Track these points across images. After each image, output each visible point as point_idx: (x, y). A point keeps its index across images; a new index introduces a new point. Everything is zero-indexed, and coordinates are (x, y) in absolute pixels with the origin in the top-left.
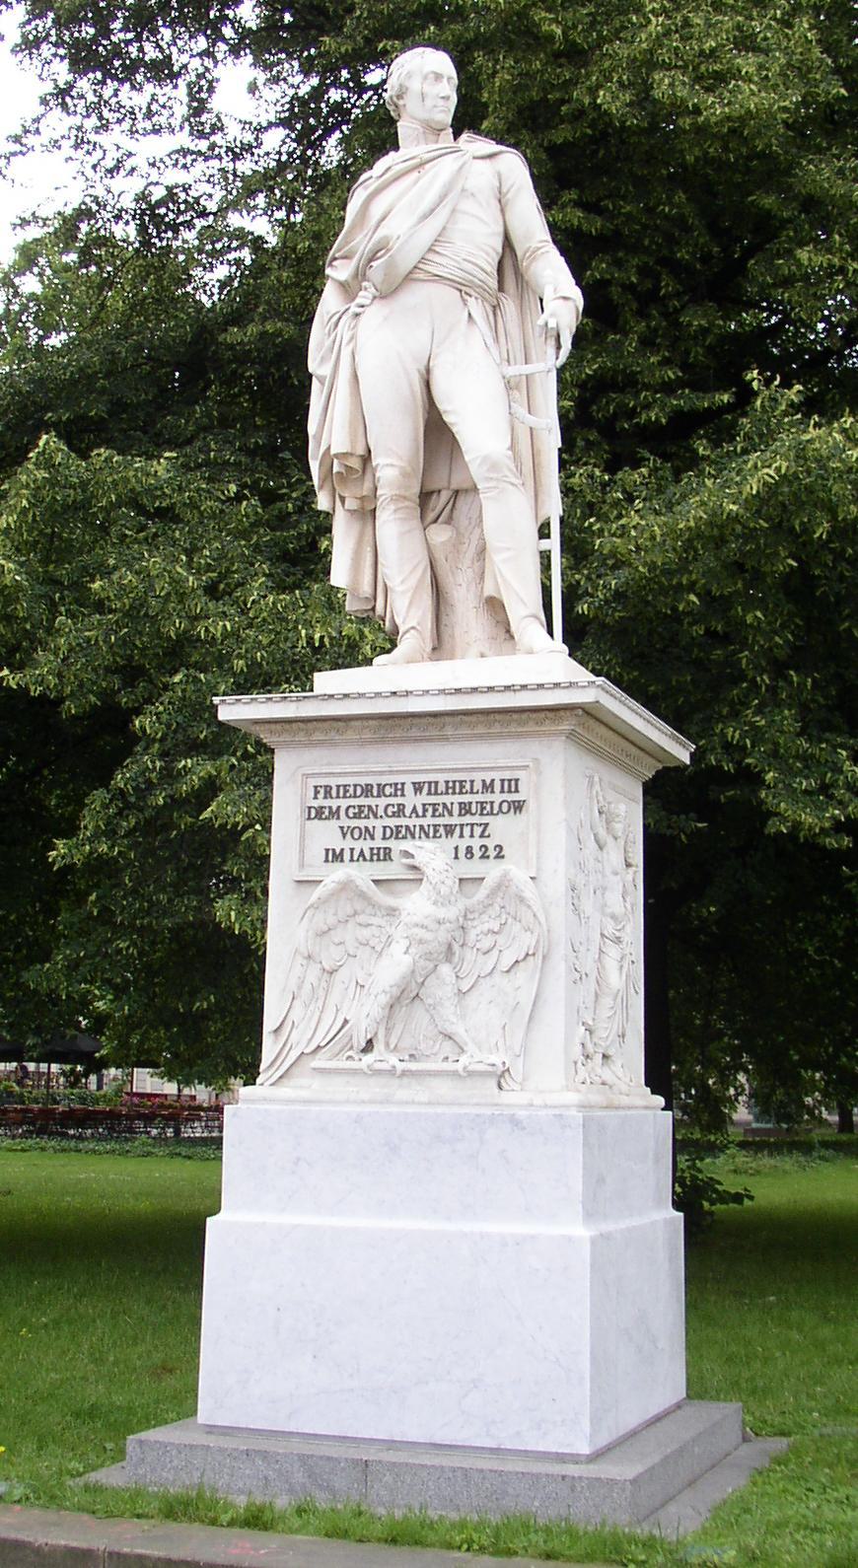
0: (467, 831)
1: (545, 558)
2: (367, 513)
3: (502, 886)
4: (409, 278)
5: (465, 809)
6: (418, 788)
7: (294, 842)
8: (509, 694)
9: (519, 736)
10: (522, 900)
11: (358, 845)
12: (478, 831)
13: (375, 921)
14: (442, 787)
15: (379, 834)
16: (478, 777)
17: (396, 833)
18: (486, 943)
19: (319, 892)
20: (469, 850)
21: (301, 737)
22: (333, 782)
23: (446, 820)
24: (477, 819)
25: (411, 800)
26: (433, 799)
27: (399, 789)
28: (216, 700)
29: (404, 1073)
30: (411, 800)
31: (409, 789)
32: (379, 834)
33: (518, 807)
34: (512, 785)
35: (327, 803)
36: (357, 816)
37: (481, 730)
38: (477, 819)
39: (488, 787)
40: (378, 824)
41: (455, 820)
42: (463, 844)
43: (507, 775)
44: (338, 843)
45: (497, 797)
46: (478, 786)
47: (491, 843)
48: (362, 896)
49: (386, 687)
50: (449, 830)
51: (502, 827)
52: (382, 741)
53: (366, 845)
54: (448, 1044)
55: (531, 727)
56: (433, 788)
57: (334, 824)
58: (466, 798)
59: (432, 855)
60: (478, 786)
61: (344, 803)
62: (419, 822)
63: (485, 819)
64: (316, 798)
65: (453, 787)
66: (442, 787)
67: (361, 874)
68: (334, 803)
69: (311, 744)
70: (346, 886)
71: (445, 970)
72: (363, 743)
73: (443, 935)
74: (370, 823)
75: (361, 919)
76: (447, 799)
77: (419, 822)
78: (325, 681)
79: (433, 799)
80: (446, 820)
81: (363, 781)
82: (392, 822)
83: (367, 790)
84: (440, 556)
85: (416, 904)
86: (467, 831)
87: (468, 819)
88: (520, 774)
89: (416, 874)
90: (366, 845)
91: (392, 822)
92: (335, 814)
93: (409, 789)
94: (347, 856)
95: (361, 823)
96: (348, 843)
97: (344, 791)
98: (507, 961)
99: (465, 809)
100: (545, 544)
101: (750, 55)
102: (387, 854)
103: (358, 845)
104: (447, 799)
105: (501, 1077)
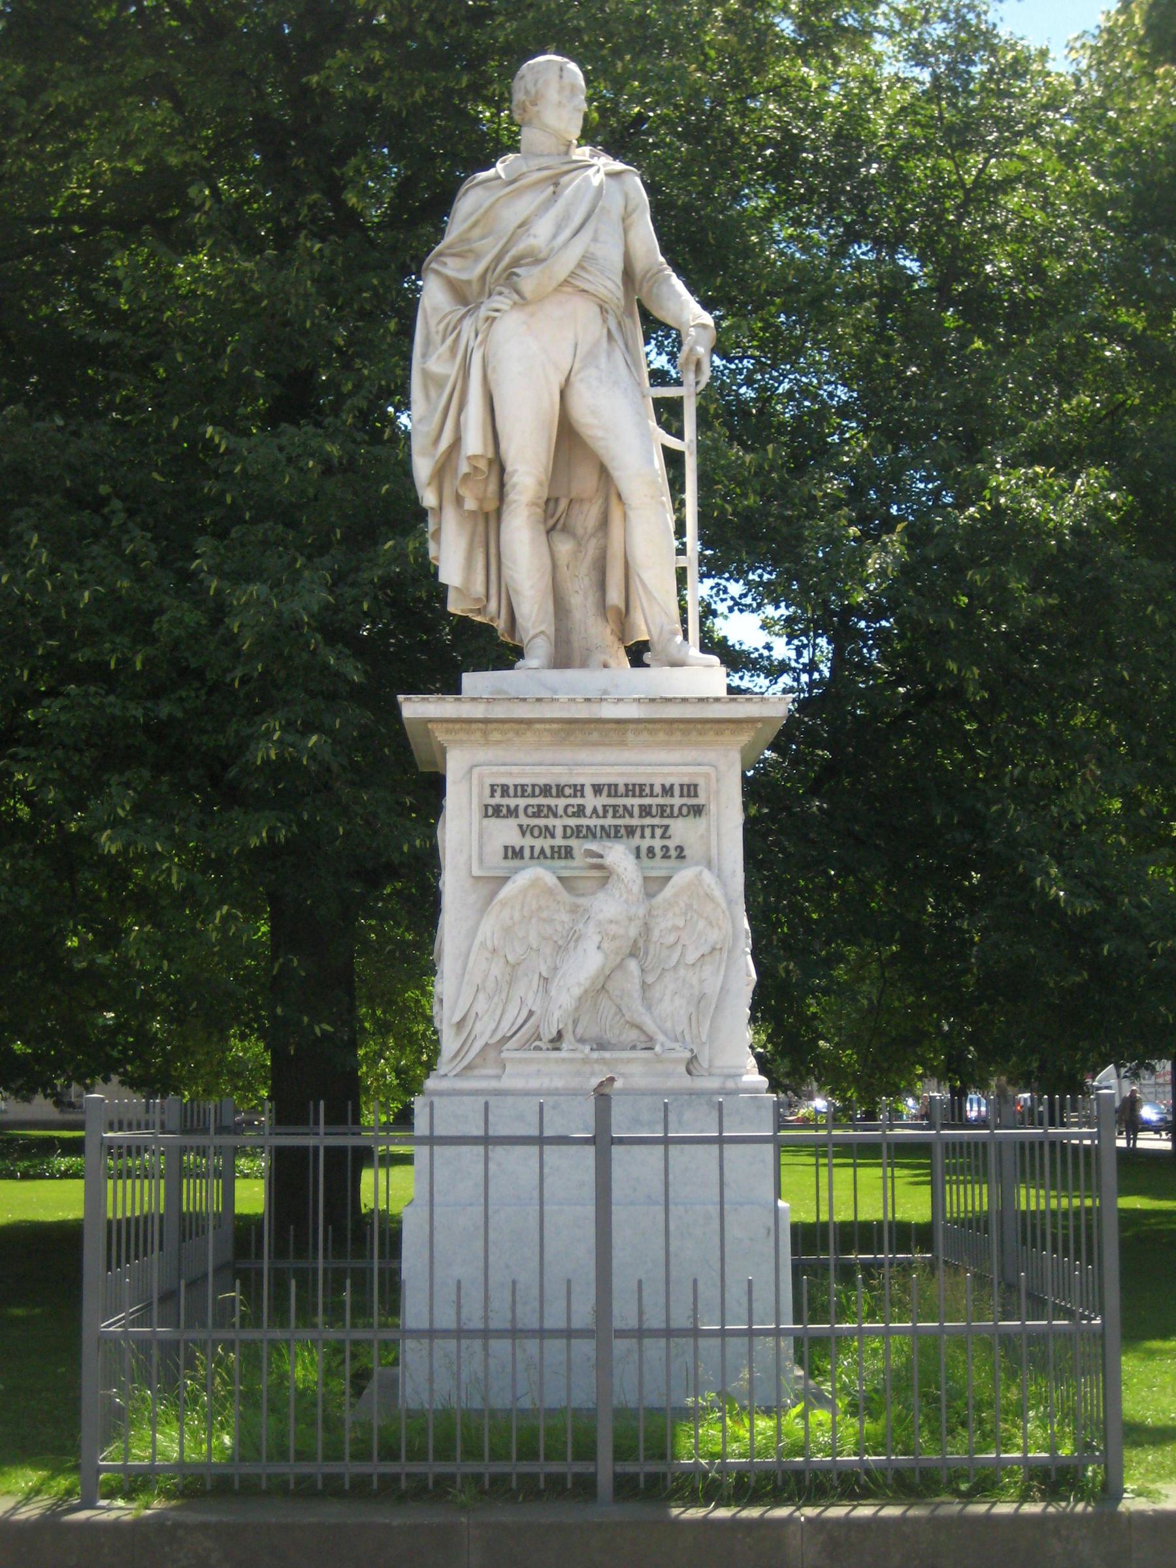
0: (648, 832)
2: (489, 520)
5: (645, 811)
6: (597, 789)
7: (463, 836)
11: (538, 843)
12: (659, 832)
14: (621, 789)
15: (559, 832)
17: (577, 832)
20: (651, 851)
22: (510, 781)
23: (627, 821)
24: (656, 821)
27: (578, 790)
28: (401, 697)
30: (591, 801)
31: (588, 791)
33: (698, 811)
35: (505, 801)
38: (656, 821)
39: (668, 791)
41: (635, 822)
42: (645, 844)
43: (686, 781)
44: (516, 840)
45: (677, 801)
50: (631, 831)
51: (682, 830)
56: (613, 790)
57: (512, 822)
58: (647, 801)
59: (618, 855)
61: (522, 802)
62: (601, 822)
63: (666, 822)
64: (492, 796)
66: (621, 789)
68: (512, 802)
71: (633, 965)
73: (633, 932)
74: (550, 822)
76: (629, 801)
77: (601, 822)
80: (627, 821)
82: (573, 822)
83: (546, 790)
85: (608, 907)
86: (648, 832)
87: (648, 821)
88: (701, 782)
89: (604, 875)
91: (573, 822)
92: (512, 812)
93: (588, 791)
94: (527, 853)
95: (541, 822)
96: (528, 841)
97: (522, 790)
99: (645, 811)
100: (683, 561)
102: (568, 853)
103: (538, 843)
104: (629, 801)
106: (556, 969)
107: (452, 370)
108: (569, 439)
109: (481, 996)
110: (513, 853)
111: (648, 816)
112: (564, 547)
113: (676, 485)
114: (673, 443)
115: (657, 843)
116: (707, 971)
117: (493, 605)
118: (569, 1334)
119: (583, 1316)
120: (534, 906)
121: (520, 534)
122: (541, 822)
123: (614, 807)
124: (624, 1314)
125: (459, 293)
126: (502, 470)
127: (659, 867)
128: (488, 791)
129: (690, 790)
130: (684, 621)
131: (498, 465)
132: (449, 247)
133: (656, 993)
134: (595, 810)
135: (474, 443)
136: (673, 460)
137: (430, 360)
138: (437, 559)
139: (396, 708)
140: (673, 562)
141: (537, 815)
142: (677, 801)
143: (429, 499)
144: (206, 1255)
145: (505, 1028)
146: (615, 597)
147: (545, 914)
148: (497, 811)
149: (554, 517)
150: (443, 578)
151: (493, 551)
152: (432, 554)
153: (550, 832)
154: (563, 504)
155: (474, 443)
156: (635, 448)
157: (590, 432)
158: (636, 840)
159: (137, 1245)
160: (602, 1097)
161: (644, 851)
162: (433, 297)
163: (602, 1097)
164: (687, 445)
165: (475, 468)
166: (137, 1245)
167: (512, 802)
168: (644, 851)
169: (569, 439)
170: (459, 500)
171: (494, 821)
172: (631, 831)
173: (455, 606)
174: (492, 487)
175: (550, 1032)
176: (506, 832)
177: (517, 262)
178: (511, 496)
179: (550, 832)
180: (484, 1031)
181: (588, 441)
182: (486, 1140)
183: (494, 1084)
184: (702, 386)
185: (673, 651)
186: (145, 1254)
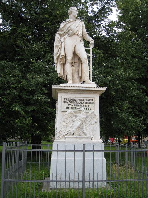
0: (86, 106)
1: (90, 72)
2: (64, 64)
3: (93, 113)
4: (74, 34)
5: (86, 103)
6: (79, 100)
7: (60, 106)
8: (94, 88)
9: (93, 94)
10: (95, 115)
11: (71, 107)
12: (88, 106)
13: (73, 117)
14: (83, 100)
15: (74, 105)
16: (88, 99)
17: (76, 105)
18: (89, 121)
19: (89, 114)
20: (86, 108)
21: (63, 92)
22: (67, 98)
23: (83, 104)
24: (87, 104)
25: (78, 101)
26: (81, 101)
27: (77, 100)
28: (52, 85)
29: (79, 138)
30: (78, 101)
31: (78, 100)
32: (74, 105)
33: (93, 103)
34: (92, 100)
35: (66, 101)
36: (70, 103)
37: (88, 93)
38: (87, 104)
39: (89, 100)
40: (74, 104)
41: (84, 104)
42: (86, 107)
43: (92, 99)
44: (68, 106)
45: (90, 102)
46: (88, 100)
47: (89, 107)
48: (73, 114)
49: (77, 86)
50: (84, 105)
51: (91, 105)
52: (74, 93)
53: (72, 107)
54: (84, 134)
55: (95, 93)
56: (81, 100)
57: (67, 104)
58: (86, 101)
59: (82, 108)
60: (88, 100)
61: (69, 101)
62: (80, 104)
63: (89, 104)
65: (84, 100)
66: (83, 100)
67: (72, 111)
68: (67, 101)
69: (64, 93)
70: (71, 112)
71: (84, 124)
72: (71, 93)
73: (84, 120)
74: (73, 104)
75: (72, 117)
76: (83, 101)
77: (80, 104)
78: (61, 85)
79: (81, 101)
80: (83, 104)
81: (72, 98)
82: (76, 104)
83: (72, 100)
84: (73, 70)
85: (81, 115)
86: (86, 106)
87: (86, 104)
88: (93, 99)
89: (80, 111)
90: (72, 107)
91: (76, 104)
92: (67, 102)
93: (78, 100)
94: (69, 108)
95: (71, 104)
96: (69, 107)
97: (69, 99)
98: (92, 123)
99: (86, 103)
100: (90, 70)
101: (19, 45)
102: (75, 108)
103: (71, 107)
104: (83, 101)
105: (92, 138)
106: (73, 124)
107: (59, 45)
108: (75, 54)
109: (63, 128)
110: (68, 108)
111: (87, 103)
112: (74, 68)
113: (89, 61)
114: (89, 55)
115: (87, 107)
116: (94, 125)
117: (64, 76)
118: (78, 181)
119: (81, 179)
120: (70, 116)
121: (68, 66)
122: (71, 104)
123: (82, 102)
124: (87, 179)
125: (60, 35)
126: (66, 58)
127: (88, 111)
128: (64, 99)
129: (92, 100)
130: (90, 78)
131: (65, 57)
132: (60, 30)
133: (87, 128)
134: (79, 103)
135: (62, 54)
136: (89, 57)
137: (56, 43)
138: (56, 70)
139: (51, 87)
140: (88, 70)
141: (71, 103)
142: (90, 102)
143: (56, 62)
144: (21, 163)
145: (66, 133)
146: (80, 75)
147: (72, 117)
148: (65, 102)
149: (73, 64)
150: (57, 72)
151: (64, 69)
152: (56, 69)
153: (73, 105)
154: (74, 63)
155: (62, 54)
156: (84, 55)
157: (77, 53)
158: (84, 107)
159: (10, 163)
160: (84, 146)
161: (85, 109)
162: (57, 36)
163: (84, 146)
164: (91, 55)
165: (63, 57)
166: (10, 163)
167: (67, 101)
168: (85, 109)
169: (75, 54)
170: (60, 62)
171: (65, 104)
172: (84, 105)
173: (59, 76)
174: (65, 60)
175: (72, 133)
176: (67, 105)
177: (69, 31)
178: (67, 61)
179: (73, 105)
180: (63, 133)
181: (77, 54)
182: (66, 151)
183: (64, 141)
184: (93, 48)
185: (89, 82)
186: (12, 165)
